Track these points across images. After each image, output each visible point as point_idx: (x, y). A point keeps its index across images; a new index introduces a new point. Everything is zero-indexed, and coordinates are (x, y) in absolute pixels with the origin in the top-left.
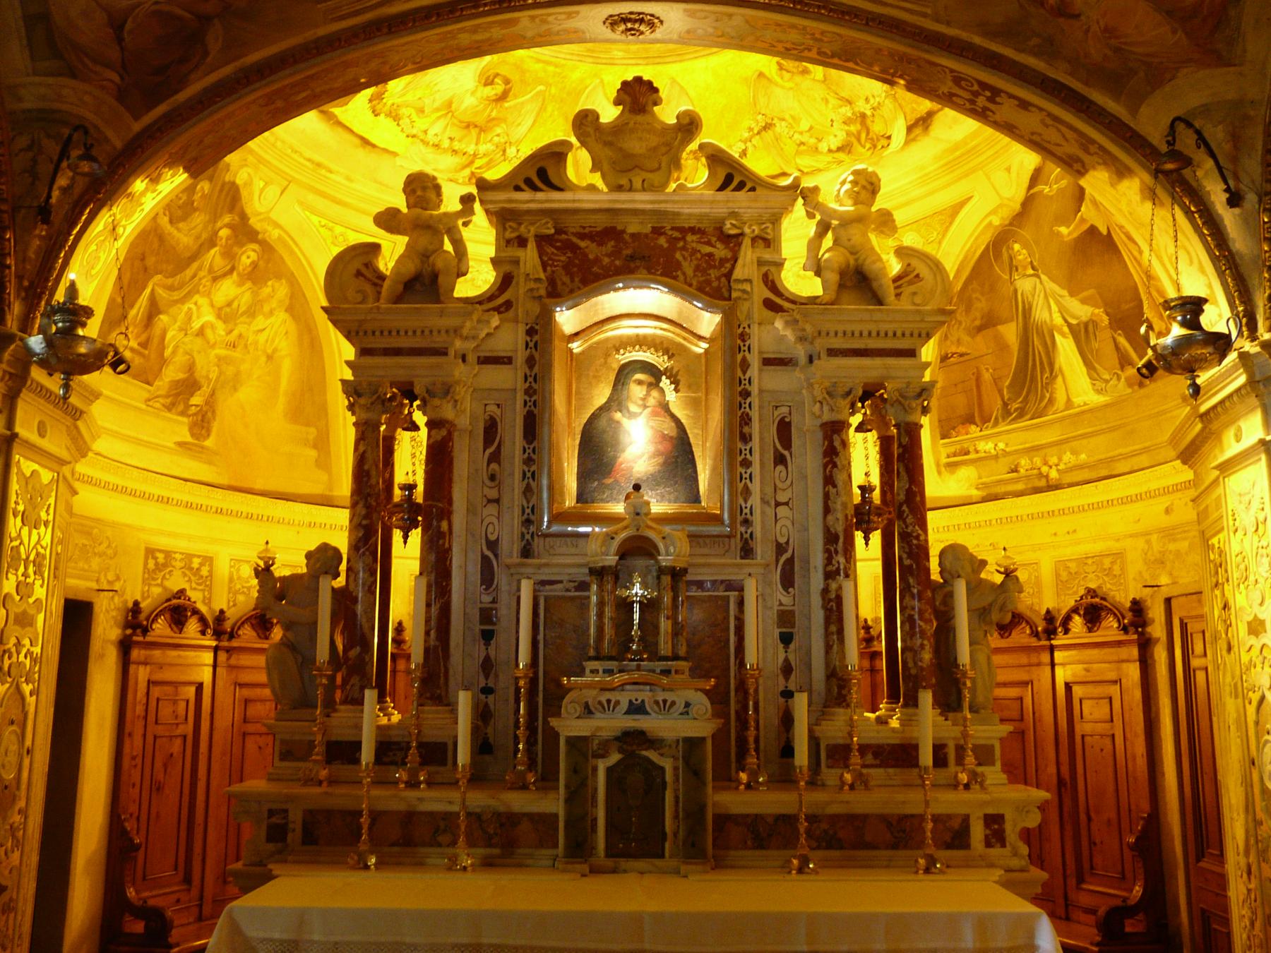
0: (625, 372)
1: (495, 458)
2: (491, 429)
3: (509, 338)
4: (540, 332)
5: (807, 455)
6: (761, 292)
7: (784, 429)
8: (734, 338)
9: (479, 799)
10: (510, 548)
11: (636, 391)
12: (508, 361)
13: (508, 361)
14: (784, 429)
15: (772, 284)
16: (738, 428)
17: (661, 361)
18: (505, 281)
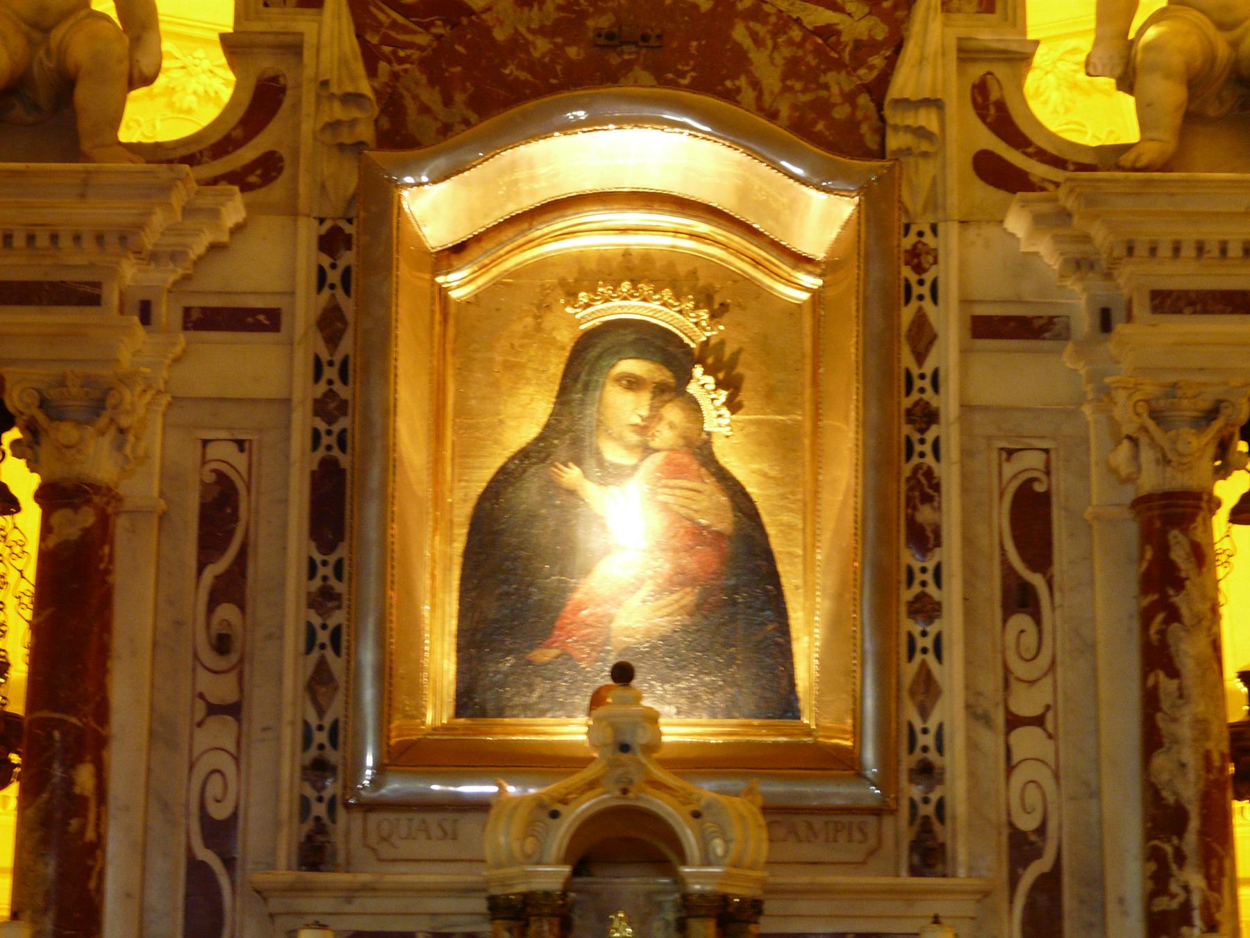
0: (588, 357)
1: (230, 588)
2: (220, 511)
3: (270, 257)
4: (358, 244)
5: (1095, 584)
6: (967, 134)
7: (1031, 514)
8: (892, 259)
9: (807, 98)
10: (268, 843)
11: (622, 407)
12: (266, 320)
13: (266, 320)
14: (1031, 514)
15: (1000, 115)
16: (902, 511)
17: (688, 324)
18: (262, 102)
